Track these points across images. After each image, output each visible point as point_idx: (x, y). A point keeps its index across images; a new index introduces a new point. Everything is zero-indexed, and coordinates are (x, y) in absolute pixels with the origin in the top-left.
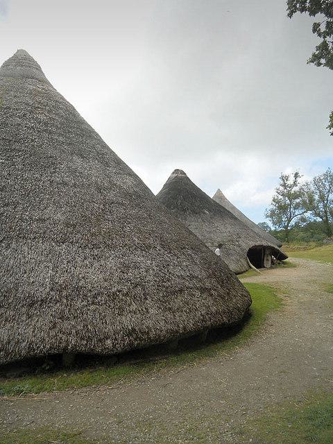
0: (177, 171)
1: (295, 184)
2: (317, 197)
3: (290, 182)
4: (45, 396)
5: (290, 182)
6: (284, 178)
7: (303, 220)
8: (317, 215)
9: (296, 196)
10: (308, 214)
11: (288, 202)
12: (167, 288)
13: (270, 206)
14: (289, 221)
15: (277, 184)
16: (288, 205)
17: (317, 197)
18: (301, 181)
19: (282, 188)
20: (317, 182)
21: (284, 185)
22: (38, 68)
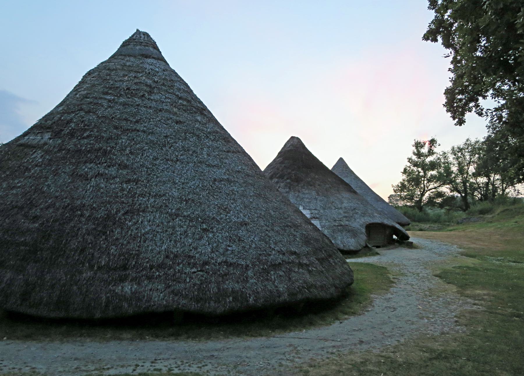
0: (292, 138)
1: (431, 152)
2: (454, 169)
3: (425, 150)
4: (142, 344)
5: (425, 150)
6: (418, 145)
7: (440, 195)
8: (455, 189)
9: (433, 166)
10: (445, 189)
11: (422, 174)
12: (158, 153)
13: (400, 178)
14: (423, 195)
15: (410, 151)
16: (422, 177)
17: (454, 169)
18: (437, 149)
19: (414, 158)
20: (457, 151)
21: (419, 155)
22: (156, 47)
